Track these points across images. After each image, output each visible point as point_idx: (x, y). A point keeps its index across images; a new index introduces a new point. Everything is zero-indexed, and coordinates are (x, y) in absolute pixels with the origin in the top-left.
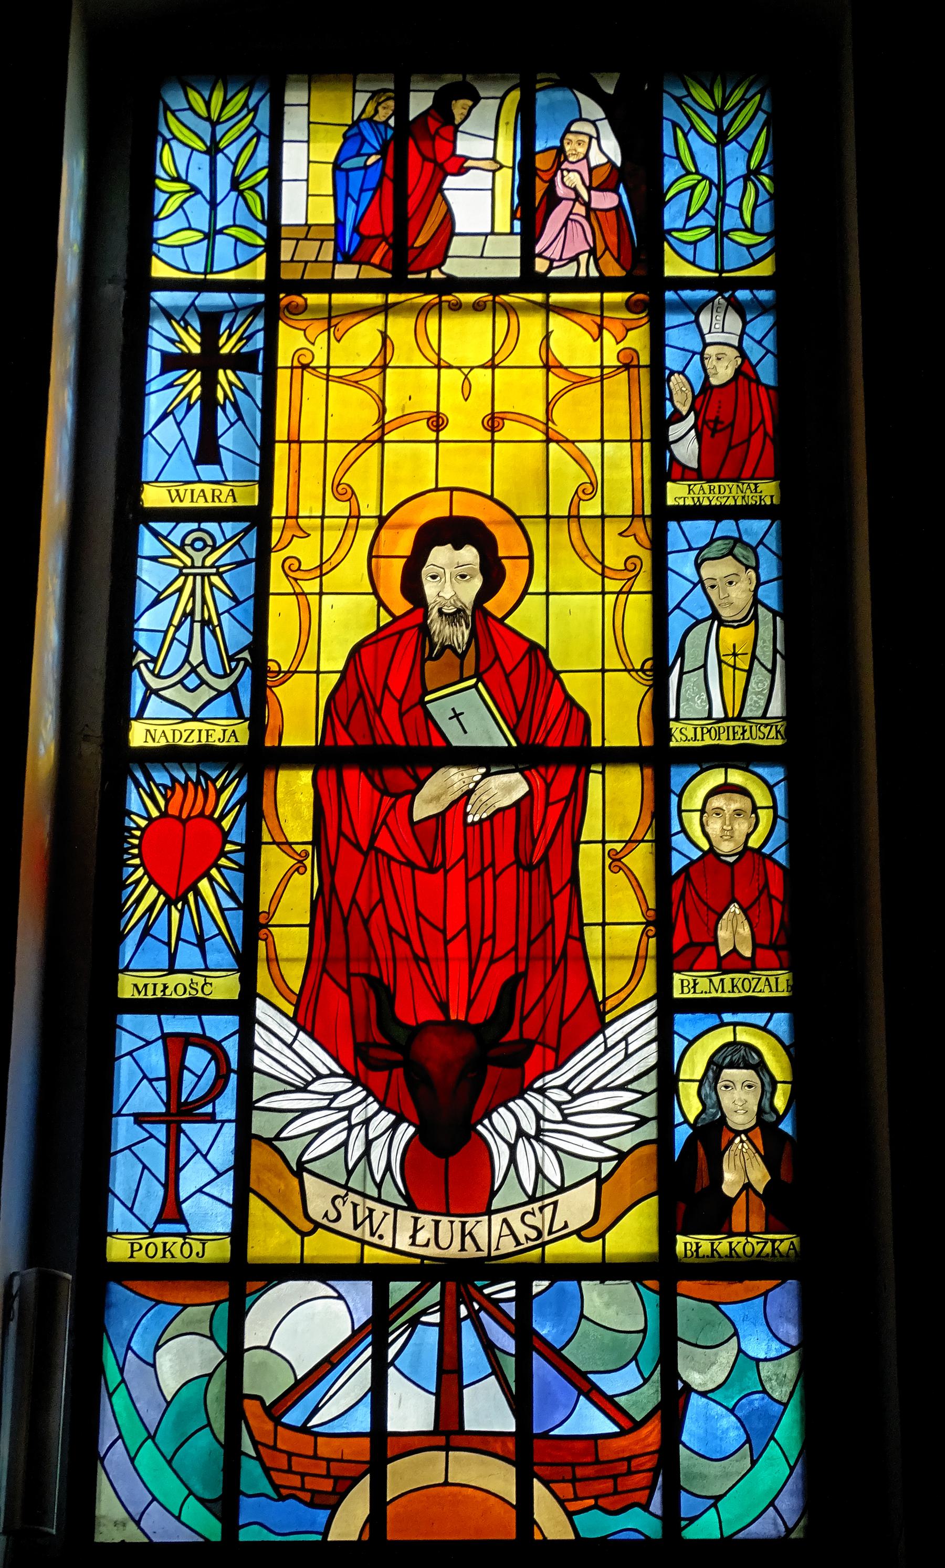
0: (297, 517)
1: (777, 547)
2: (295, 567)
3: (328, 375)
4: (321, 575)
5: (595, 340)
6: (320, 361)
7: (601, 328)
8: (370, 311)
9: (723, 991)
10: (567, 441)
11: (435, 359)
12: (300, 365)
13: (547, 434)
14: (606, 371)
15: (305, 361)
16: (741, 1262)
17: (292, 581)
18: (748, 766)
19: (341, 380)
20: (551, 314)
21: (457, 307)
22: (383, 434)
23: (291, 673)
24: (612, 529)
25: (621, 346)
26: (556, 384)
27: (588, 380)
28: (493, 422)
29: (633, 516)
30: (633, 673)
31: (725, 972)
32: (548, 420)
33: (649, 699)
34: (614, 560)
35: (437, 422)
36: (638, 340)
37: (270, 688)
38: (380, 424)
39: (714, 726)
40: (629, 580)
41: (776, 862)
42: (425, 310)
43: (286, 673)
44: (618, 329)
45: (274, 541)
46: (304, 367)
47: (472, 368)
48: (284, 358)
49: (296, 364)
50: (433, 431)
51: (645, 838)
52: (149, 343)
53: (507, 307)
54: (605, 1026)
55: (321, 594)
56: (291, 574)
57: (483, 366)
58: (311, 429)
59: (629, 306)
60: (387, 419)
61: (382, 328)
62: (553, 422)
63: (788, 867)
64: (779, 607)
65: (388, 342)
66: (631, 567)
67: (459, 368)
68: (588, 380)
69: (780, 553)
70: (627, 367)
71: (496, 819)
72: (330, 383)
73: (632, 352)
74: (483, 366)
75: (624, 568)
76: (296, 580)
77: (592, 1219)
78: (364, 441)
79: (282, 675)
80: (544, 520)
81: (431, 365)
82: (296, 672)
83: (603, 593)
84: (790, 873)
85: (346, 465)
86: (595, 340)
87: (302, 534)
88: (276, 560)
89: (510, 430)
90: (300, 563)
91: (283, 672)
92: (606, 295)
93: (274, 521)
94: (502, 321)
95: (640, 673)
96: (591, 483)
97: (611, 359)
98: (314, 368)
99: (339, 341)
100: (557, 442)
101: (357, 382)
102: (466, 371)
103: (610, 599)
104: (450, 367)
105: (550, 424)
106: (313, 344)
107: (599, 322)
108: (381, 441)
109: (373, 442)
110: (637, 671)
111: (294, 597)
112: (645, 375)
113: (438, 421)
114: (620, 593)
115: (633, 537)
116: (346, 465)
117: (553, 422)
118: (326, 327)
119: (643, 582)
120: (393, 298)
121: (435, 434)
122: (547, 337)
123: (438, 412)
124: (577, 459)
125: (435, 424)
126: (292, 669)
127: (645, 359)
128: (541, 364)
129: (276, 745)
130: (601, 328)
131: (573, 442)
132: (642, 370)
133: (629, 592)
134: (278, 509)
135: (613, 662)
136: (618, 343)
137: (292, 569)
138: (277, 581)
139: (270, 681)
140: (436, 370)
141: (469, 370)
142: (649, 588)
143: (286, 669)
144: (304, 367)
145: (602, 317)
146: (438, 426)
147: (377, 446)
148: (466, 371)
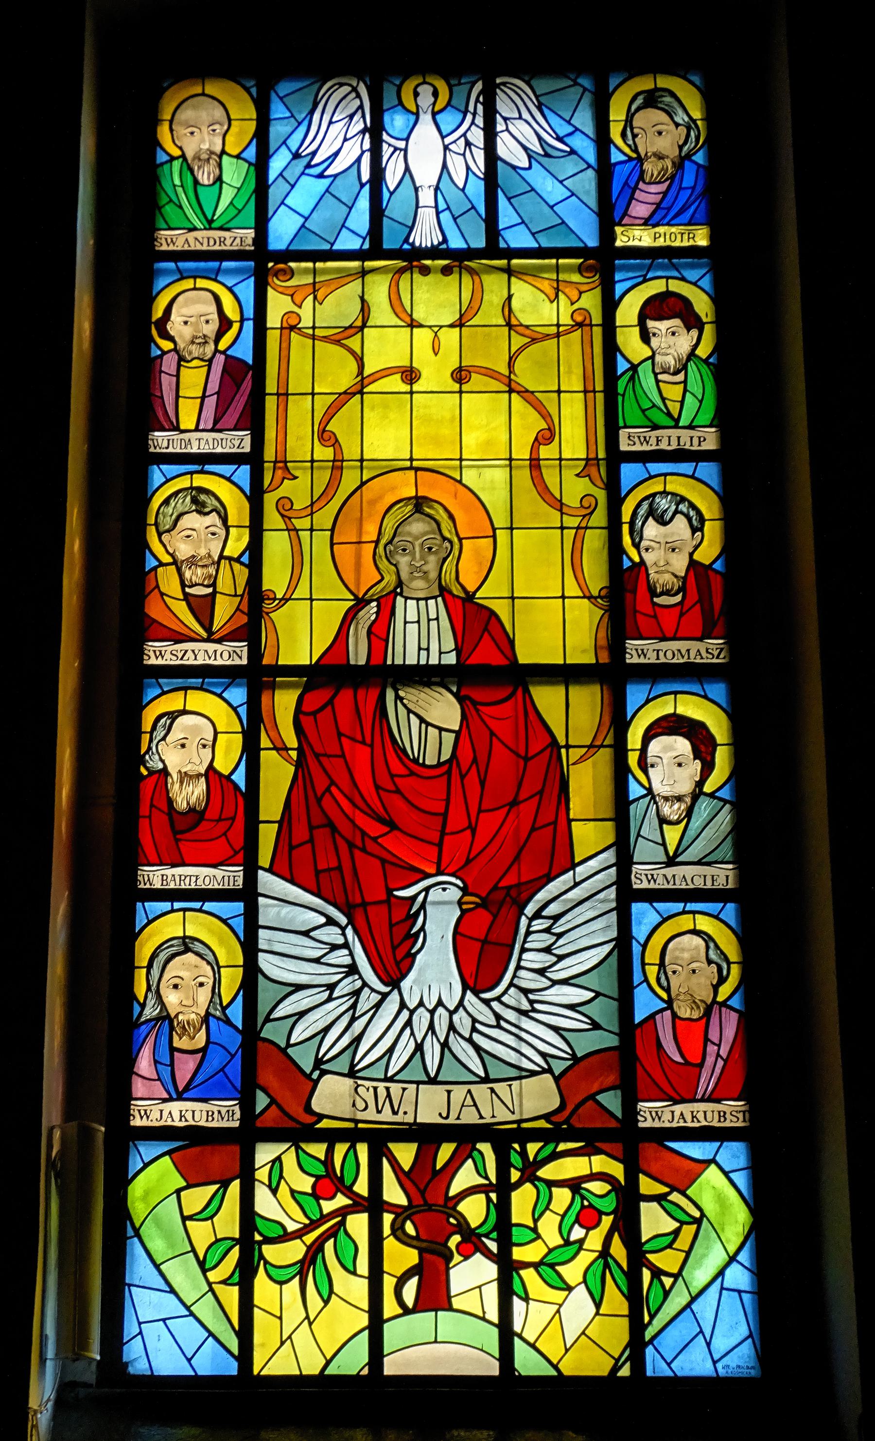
0: (286, 462)
1: (727, 702)
2: (288, 507)
3: (314, 335)
4: (312, 514)
5: (552, 302)
6: (306, 322)
7: (557, 290)
8: (347, 276)
9: (674, 884)
10: (527, 391)
11: (408, 320)
12: (288, 326)
13: (509, 385)
14: (561, 329)
15: (293, 322)
16: (689, 889)
17: (287, 519)
18: (686, 74)
19: (325, 339)
20: (513, 279)
21: (425, 271)
22: (363, 388)
23: (285, 600)
24: (569, 475)
25: (576, 306)
26: (518, 341)
27: (547, 337)
28: (461, 375)
29: (587, 460)
30: (593, 600)
31: (676, 1102)
32: (510, 372)
33: (606, 619)
34: (572, 499)
35: (410, 375)
36: (591, 302)
37: (267, 614)
38: (359, 378)
39: (663, 871)
40: (584, 516)
41: (714, 570)
42: (401, 271)
43: (281, 600)
44: (574, 294)
45: (266, 482)
46: (292, 328)
47: (441, 327)
48: (273, 319)
49: (285, 325)
50: (408, 384)
51: (605, 743)
52: (276, 88)
53: (470, 270)
54: (573, 866)
55: (312, 530)
56: (285, 513)
57: (452, 326)
58: (298, 382)
59: (580, 269)
60: (366, 374)
61: (360, 292)
62: (515, 375)
63: (743, 1010)
64: (705, 162)
65: (366, 305)
66: (586, 504)
67: (430, 327)
68: (547, 337)
69: (721, 493)
70: (580, 325)
71: (451, 872)
72: (316, 341)
73: (585, 313)
74: (452, 326)
75: (579, 506)
76: (290, 518)
77: (561, 1102)
78: (345, 393)
79: (277, 602)
80: (508, 457)
81: (404, 324)
82: (290, 599)
83: (562, 528)
84: (724, 576)
85: (331, 412)
86: (552, 302)
87: (291, 477)
88: (270, 500)
89: (477, 381)
90: (292, 504)
91: (278, 599)
92: (561, 261)
93: (266, 465)
94: (467, 279)
95: (599, 600)
96: (549, 429)
97: (565, 319)
98: (299, 329)
99: (321, 304)
100: (518, 392)
101: (339, 341)
102: (436, 329)
103: (570, 534)
104: (421, 326)
105: (512, 376)
106: (300, 307)
107: (555, 286)
108: (361, 393)
109: (354, 394)
110: (596, 598)
111: (286, 532)
112: (598, 332)
113: (411, 375)
114: (578, 528)
115: (587, 478)
116: (331, 412)
117: (515, 375)
118: (312, 291)
119: (600, 517)
120: (369, 264)
121: (409, 387)
122: (510, 297)
123: (411, 367)
124: (536, 406)
125: (409, 378)
126: (287, 596)
127: (597, 319)
128: (505, 324)
129: (274, 663)
130: (557, 290)
131: (532, 392)
132: (594, 328)
133: (586, 528)
134: (269, 453)
135: (572, 589)
136: (572, 304)
137: (285, 508)
138: (272, 518)
139: (267, 606)
140: (409, 329)
141: (438, 328)
142: (604, 523)
143: (281, 597)
144: (292, 328)
145: (558, 281)
146: (411, 380)
147: (358, 396)
148: (436, 329)
